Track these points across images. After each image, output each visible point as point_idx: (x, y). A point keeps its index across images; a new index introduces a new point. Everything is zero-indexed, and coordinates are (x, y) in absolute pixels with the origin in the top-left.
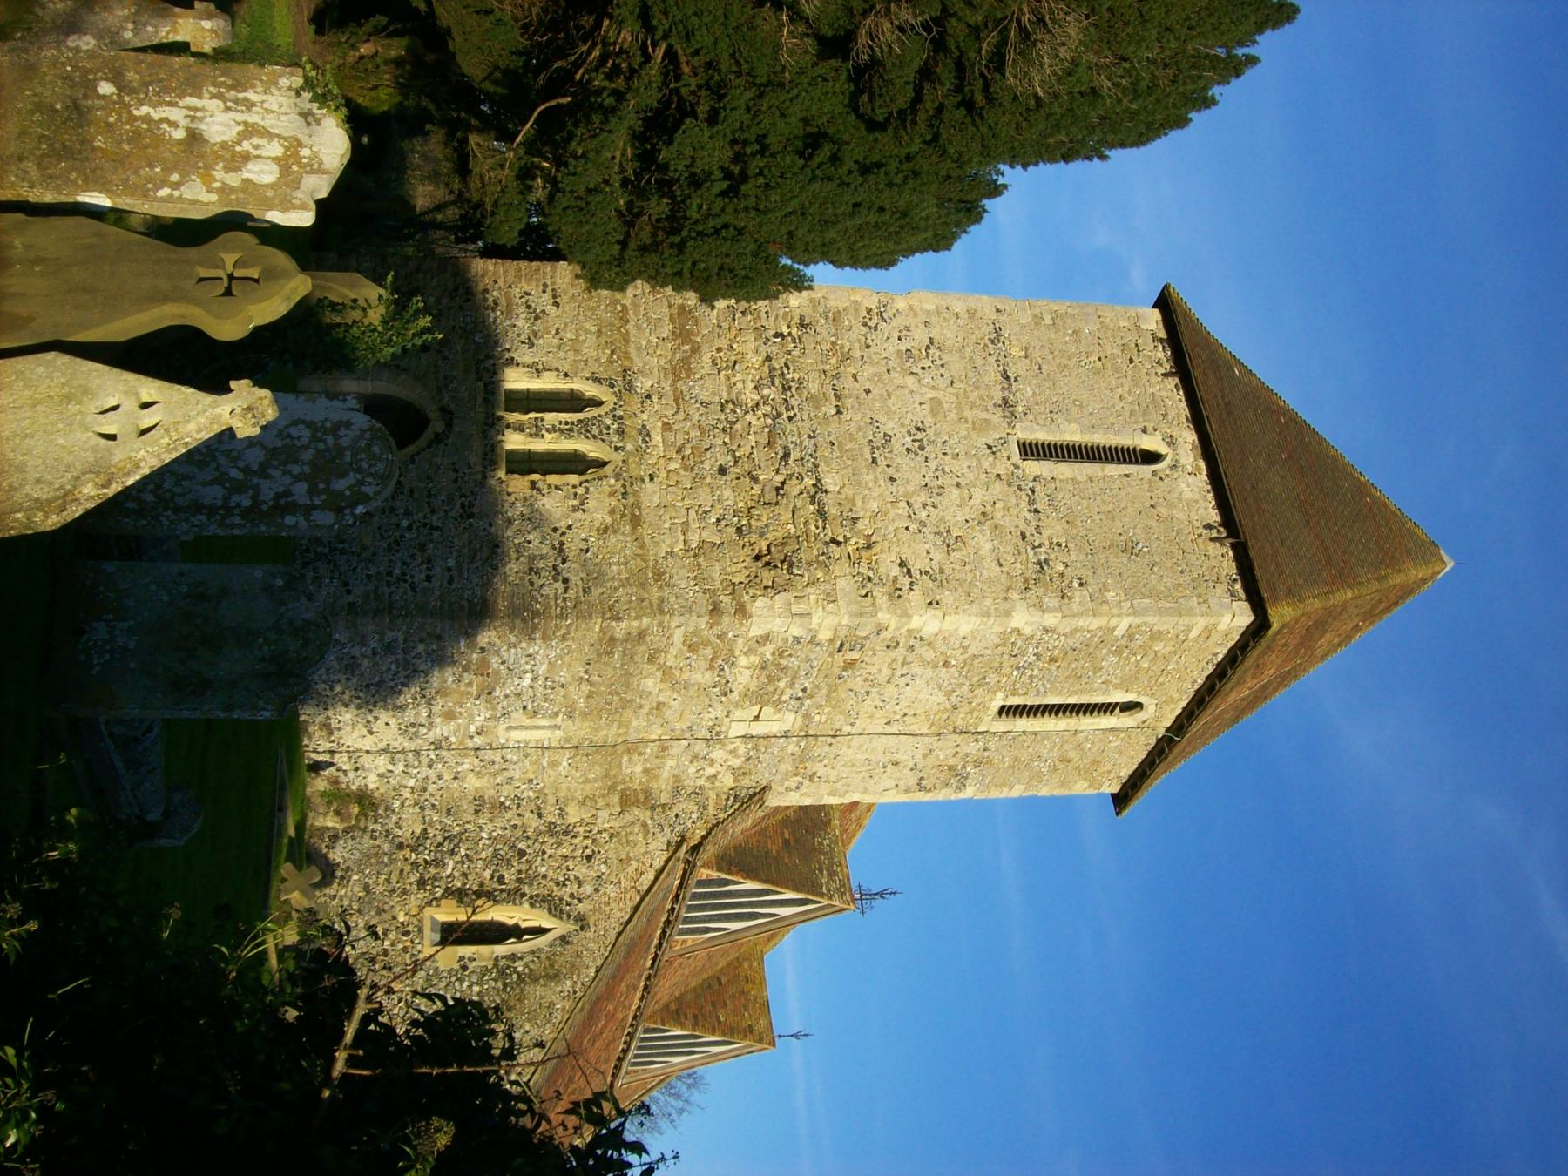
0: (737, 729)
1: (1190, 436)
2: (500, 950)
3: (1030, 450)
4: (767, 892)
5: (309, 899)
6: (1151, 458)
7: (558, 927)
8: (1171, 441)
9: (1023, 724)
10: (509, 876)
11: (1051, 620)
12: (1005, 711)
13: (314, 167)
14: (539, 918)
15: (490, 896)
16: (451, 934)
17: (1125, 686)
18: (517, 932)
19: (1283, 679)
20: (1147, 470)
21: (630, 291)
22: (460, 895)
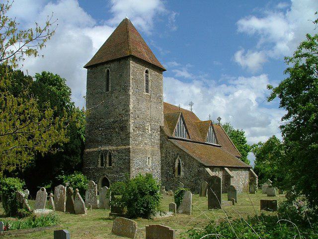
0: (150, 132)
1: (105, 66)
2: (181, 166)
3: (107, 90)
4: (178, 125)
5: (244, 190)
6: (108, 71)
7: (178, 157)
8: (106, 68)
9: (150, 89)
10: (172, 165)
11: (131, 88)
12: (147, 91)
13: (237, 174)
14: (177, 162)
15: (174, 167)
16: (179, 173)
17: (142, 74)
18: (179, 164)
19: (145, 45)
20: (110, 72)
21: (214, 102)
22: (174, 172)
